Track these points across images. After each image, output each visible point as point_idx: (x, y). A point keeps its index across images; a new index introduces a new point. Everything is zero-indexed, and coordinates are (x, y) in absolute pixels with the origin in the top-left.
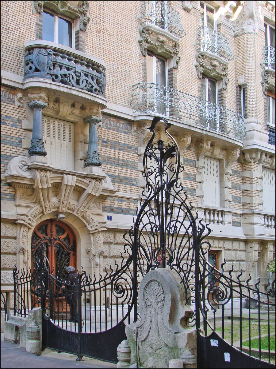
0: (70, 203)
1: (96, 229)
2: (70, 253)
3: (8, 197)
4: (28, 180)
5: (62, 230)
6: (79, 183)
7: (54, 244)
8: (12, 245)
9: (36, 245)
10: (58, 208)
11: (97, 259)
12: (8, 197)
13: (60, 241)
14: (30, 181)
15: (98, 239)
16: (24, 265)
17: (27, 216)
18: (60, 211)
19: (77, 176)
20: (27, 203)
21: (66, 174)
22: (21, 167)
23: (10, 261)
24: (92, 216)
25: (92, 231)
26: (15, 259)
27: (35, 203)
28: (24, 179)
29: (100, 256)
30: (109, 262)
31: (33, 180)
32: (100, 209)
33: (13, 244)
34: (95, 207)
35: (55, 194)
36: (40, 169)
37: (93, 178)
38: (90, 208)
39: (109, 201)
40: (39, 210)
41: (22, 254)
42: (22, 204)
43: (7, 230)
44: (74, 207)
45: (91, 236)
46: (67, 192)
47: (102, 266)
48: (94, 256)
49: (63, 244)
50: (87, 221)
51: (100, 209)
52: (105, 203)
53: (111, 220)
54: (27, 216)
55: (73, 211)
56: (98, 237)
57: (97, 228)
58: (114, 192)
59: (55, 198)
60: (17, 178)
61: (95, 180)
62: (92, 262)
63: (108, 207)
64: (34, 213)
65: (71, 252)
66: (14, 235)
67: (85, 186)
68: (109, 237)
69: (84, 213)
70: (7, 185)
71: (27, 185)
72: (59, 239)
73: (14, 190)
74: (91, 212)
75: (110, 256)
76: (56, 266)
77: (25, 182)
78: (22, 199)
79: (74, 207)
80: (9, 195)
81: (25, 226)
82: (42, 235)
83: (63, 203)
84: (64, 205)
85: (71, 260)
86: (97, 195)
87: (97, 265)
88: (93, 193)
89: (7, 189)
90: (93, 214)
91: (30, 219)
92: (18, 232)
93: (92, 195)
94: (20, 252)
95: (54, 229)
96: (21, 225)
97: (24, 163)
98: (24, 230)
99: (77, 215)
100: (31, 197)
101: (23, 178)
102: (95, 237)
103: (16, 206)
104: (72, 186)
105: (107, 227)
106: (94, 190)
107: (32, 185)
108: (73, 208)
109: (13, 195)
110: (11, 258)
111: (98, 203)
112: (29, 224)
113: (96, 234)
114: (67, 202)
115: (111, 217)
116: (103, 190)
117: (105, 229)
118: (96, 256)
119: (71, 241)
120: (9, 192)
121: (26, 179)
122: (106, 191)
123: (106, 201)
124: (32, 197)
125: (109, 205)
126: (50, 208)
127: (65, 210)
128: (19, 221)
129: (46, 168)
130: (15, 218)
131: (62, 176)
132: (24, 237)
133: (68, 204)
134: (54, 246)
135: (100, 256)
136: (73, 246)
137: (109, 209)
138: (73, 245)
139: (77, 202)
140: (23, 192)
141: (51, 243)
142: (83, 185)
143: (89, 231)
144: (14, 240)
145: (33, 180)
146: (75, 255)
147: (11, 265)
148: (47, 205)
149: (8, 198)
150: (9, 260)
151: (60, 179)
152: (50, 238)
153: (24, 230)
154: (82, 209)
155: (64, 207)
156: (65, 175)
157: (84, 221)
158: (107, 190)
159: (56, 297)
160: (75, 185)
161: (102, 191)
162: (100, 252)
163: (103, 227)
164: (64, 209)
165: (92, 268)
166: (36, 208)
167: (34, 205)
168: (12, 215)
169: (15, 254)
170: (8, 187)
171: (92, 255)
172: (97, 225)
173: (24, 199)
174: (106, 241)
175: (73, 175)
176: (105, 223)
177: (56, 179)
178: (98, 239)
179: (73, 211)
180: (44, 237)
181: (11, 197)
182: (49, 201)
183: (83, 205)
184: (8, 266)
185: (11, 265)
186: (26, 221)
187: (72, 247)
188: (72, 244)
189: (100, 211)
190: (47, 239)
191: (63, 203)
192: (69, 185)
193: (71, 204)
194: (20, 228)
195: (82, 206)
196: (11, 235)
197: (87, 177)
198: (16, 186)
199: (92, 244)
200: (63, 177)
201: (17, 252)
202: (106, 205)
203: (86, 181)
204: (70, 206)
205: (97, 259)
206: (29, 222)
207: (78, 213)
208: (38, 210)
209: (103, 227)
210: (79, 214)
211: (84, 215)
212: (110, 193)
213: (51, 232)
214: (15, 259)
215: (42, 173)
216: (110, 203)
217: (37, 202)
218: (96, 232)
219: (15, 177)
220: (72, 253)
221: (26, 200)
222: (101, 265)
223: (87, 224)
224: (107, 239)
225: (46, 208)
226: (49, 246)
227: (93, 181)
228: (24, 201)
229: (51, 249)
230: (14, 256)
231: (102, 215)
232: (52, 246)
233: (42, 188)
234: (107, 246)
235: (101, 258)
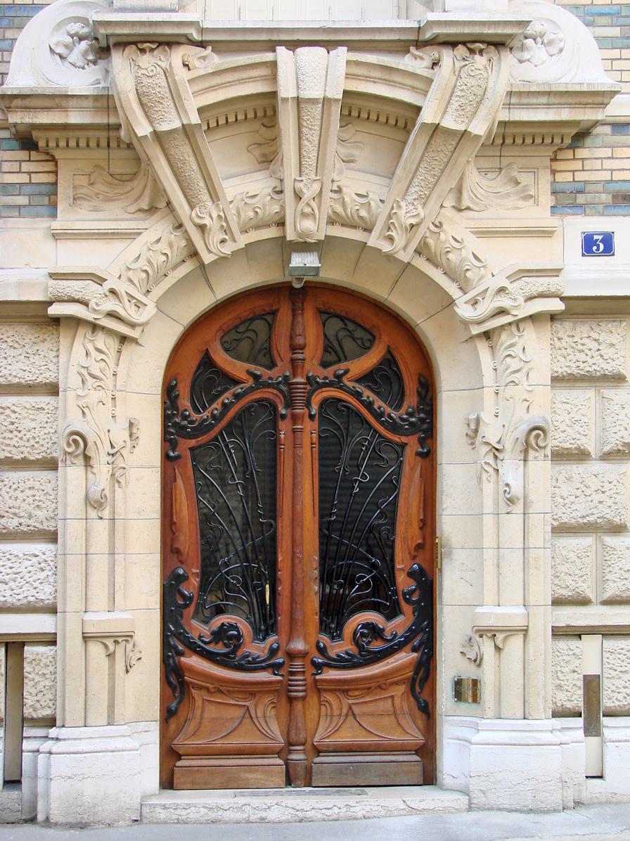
0: (339, 191)
1: (502, 312)
2: (403, 446)
3: (22, 200)
4: (85, 103)
5: (359, 334)
6: (367, 79)
7: (308, 405)
8: (33, 425)
9: (214, 416)
10: (281, 224)
11: (511, 471)
12: (22, 200)
13: (343, 388)
14: (97, 109)
15: (514, 364)
16: (93, 514)
17: (100, 280)
18: (291, 236)
19: (352, 46)
20: (114, 216)
21: (293, 45)
22: (60, 50)
23: (21, 496)
24: (473, 244)
25: (480, 323)
26: (49, 488)
27: (152, 210)
28: (64, 103)
29: (526, 451)
30: (594, 483)
31: (106, 101)
32: (537, 203)
33: (42, 417)
34: (508, 195)
35: (264, 155)
36: (464, 43)
37: (453, 44)
38: (466, 202)
39: (606, 152)
40: (171, 245)
41: (81, 461)
42: (78, 225)
43: (11, 352)
44: (369, 211)
45: (482, 348)
46: (312, 135)
47: (540, 501)
48: (496, 451)
49: (362, 402)
50: (449, 273)
51: (537, 203)
52: (578, 165)
53: (609, 249)
54: (100, 280)
55: (368, 230)
56: (516, 351)
57: (504, 302)
58: (600, 98)
59: (258, 176)
60: (27, 102)
61: (461, 50)
62: (488, 488)
63: (599, 187)
64: (142, 263)
65: (404, 439)
66: (46, 377)
67: (413, 88)
68: (594, 346)
69: (422, 231)
70: (15, 144)
71: (224, 110)
72: (339, 377)
73: (49, 166)
74: (473, 224)
75: (606, 449)
76: (324, 512)
77: (74, 118)
78: (85, 204)
79: (369, 211)
80: (26, 189)
81: (95, 327)
82: (252, 367)
83: (298, 197)
84: (302, 204)
85: (404, 481)
86: (479, 127)
87: (511, 501)
88: (449, 123)
89: (15, 167)
90: (482, 233)
91: (113, 292)
92: (63, 359)
93: (450, 133)
94: (66, 453)
95: (311, 332)
96: (76, 322)
97: (76, 28)
98: (90, 347)
99: (386, 247)
100: (129, 186)
101: (59, 100)
102: (501, 353)
103: (56, 236)
104: (326, 101)
105: (568, 293)
106: (455, 104)
107: (109, 127)
108: (363, 213)
109: (44, 189)
110: (30, 483)
111: (523, 169)
112: (112, 315)
113: (504, 336)
114: (316, 187)
115: (608, 241)
116: (516, 96)
117: (557, 306)
118: (506, 455)
119: (411, 386)
120: (24, 178)
121: (73, 103)
122: (544, 100)
123: (581, 153)
124: (137, 184)
125: (606, 176)
126: (227, 230)
127: (314, 228)
128: (54, 310)
129: (159, 31)
130: (39, 297)
131: (268, 57)
132: (90, 380)
133: (327, 194)
134: (311, 417)
135: (526, 451)
136: (419, 411)
137: (606, 198)
138: (419, 403)
139: (385, 181)
140: (88, 170)
141: (289, 404)
142: (402, 86)
143: (466, 324)
144: (44, 400)
145: (106, 101)
146: (429, 455)
147: (30, 517)
148: (208, 214)
149: (19, 207)
150: (18, 493)
151: (264, 78)
152: (286, 378)
153: (90, 347)
154: (406, 215)
155: (304, 215)
156: (281, 50)
157: (436, 275)
158: (549, 93)
159: (319, 667)
160: (346, 93)
161: (509, 106)
162: (525, 427)
163: (542, 295)
164: (308, 225)
165: (489, 521)
166: (149, 237)
167: (141, 225)
168: (20, 285)
169: (51, 465)
170: (23, 155)
171: (488, 448)
172: (502, 290)
173: (95, 203)
174: (575, 371)
175: (329, 45)
176: (556, 272)
177: (241, 82)
178: (514, 364)
179: (368, 230)
180: (256, 377)
181: (37, 200)
182: (214, 196)
183: (412, 190)
184: (15, 522)
185: (30, 517)
186: (92, 304)
187: (411, 415)
188: (411, 401)
189: (539, 213)
190: (269, 386)
191: (298, 197)
192: (313, 101)
193: (349, 194)
194: (69, 340)
195: (409, 198)
196: (28, 378)
197: (420, 44)
198: (52, 144)
199: (488, 394)
200: (274, 65)
201: (57, 454)
202: (580, 176)
203: (415, 63)
204: (344, 204)
205: (511, 471)
206: (111, 305)
207: (391, 239)
208: (163, 247)
209: (542, 295)
210: (400, 240)
211: (431, 241)
212: (572, 106)
213: (294, 348)
214: (49, 488)
215: (146, 61)
216: (608, 164)
217: (158, 205)
218: (502, 327)
219: (18, 102)
220: (412, 445)
221: (106, 206)
222: (532, 497)
223: (452, 289)
224: (582, 357)
225: (202, 228)
226: (283, 417)
227: (447, 56)
228: (96, 210)
229: (294, 431)
230: (46, 475)
231: (546, 233)
232: (295, 419)
233: (157, 135)
234: (584, 397)
235: (531, 463)
